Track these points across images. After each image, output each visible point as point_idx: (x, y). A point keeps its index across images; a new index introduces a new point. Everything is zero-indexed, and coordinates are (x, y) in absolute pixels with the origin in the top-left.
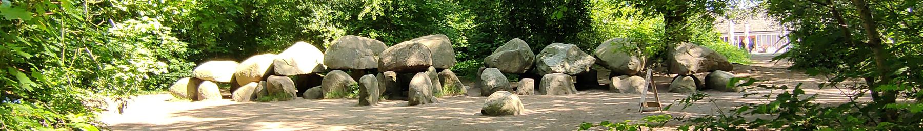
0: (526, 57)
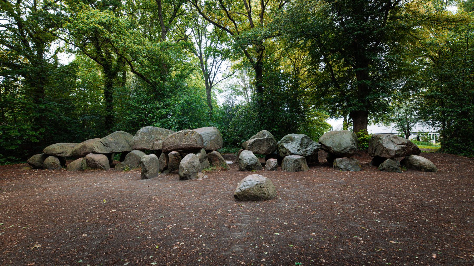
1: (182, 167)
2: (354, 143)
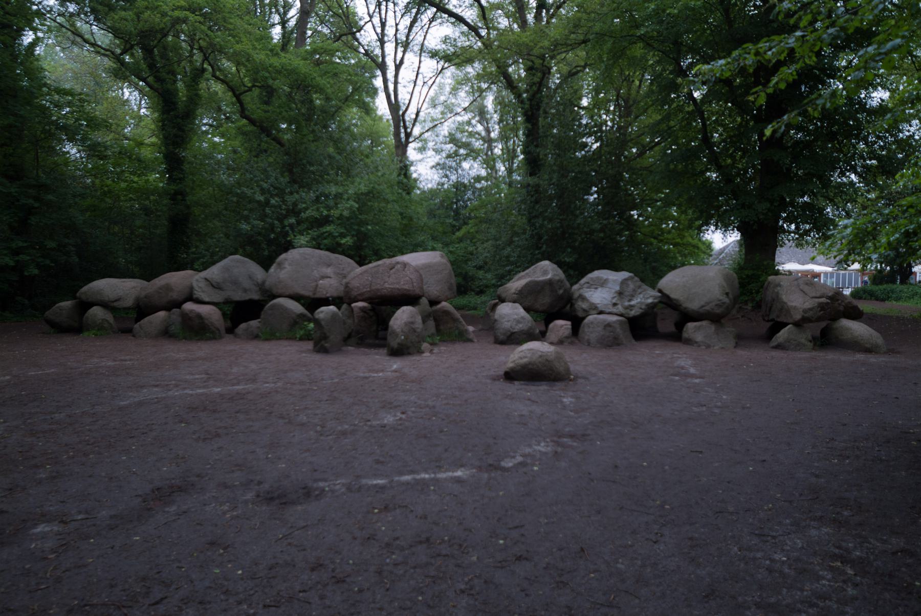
0: (560, 289)
1: (394, 332)
2: (727, 294)
